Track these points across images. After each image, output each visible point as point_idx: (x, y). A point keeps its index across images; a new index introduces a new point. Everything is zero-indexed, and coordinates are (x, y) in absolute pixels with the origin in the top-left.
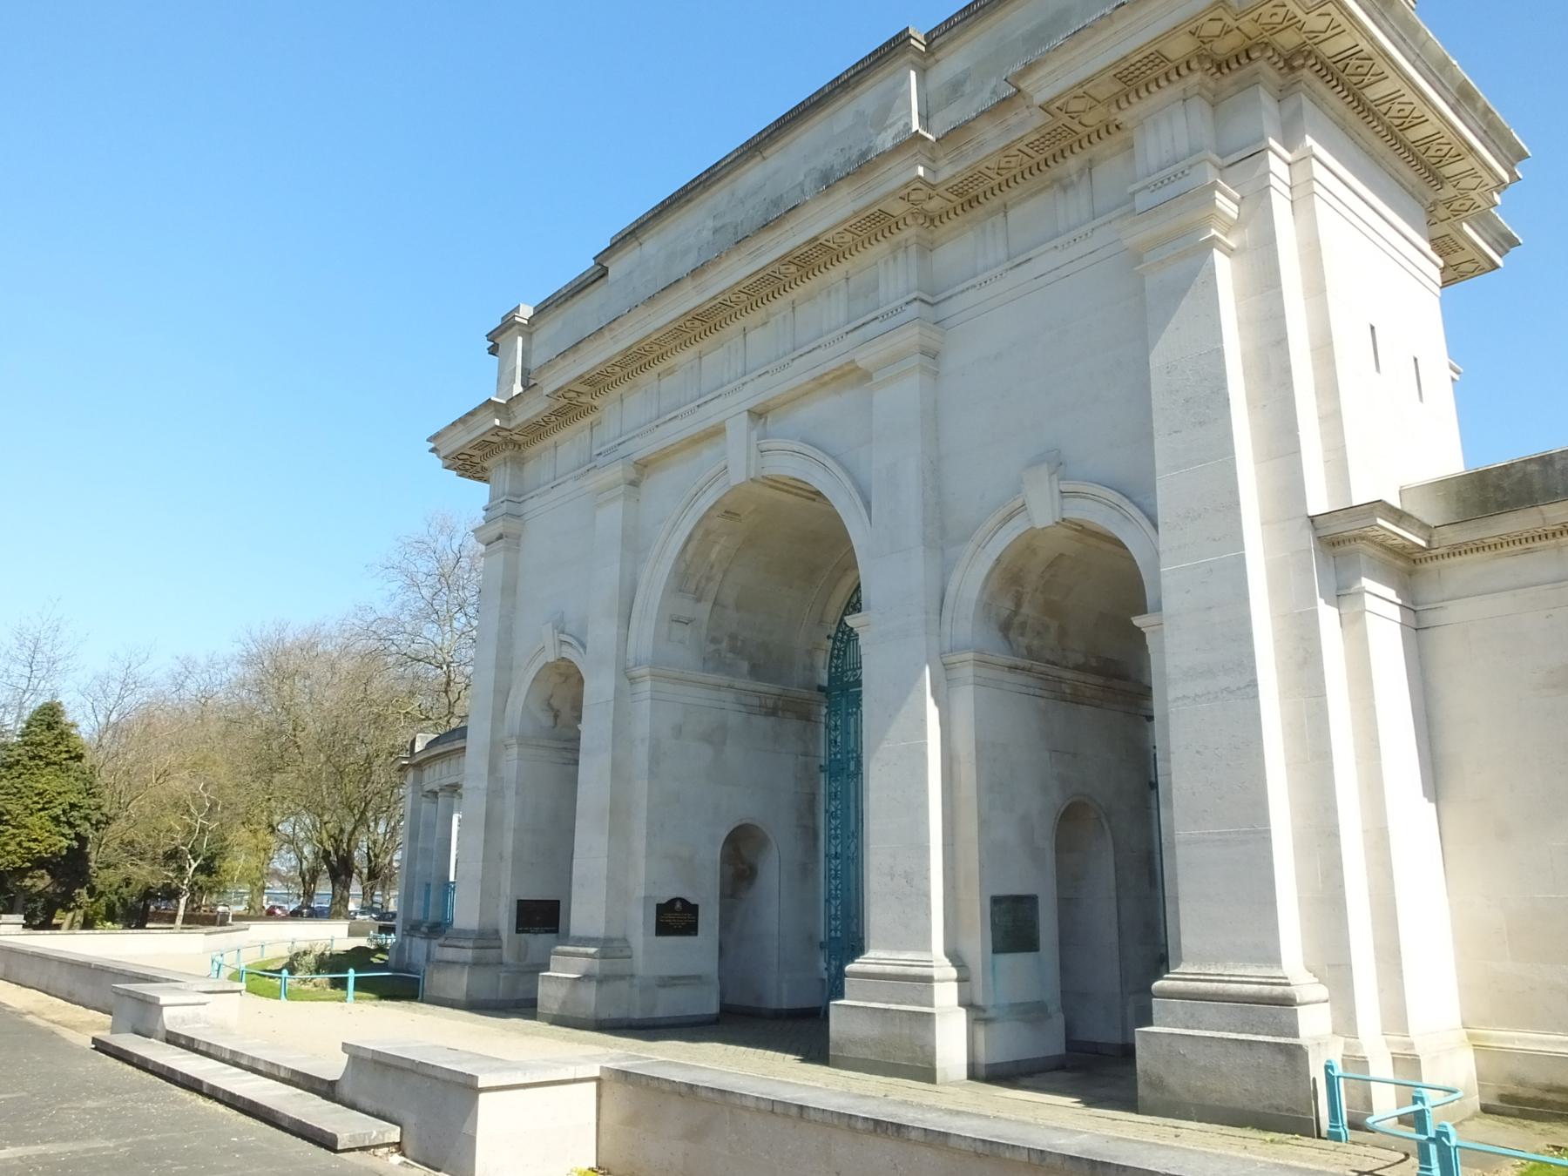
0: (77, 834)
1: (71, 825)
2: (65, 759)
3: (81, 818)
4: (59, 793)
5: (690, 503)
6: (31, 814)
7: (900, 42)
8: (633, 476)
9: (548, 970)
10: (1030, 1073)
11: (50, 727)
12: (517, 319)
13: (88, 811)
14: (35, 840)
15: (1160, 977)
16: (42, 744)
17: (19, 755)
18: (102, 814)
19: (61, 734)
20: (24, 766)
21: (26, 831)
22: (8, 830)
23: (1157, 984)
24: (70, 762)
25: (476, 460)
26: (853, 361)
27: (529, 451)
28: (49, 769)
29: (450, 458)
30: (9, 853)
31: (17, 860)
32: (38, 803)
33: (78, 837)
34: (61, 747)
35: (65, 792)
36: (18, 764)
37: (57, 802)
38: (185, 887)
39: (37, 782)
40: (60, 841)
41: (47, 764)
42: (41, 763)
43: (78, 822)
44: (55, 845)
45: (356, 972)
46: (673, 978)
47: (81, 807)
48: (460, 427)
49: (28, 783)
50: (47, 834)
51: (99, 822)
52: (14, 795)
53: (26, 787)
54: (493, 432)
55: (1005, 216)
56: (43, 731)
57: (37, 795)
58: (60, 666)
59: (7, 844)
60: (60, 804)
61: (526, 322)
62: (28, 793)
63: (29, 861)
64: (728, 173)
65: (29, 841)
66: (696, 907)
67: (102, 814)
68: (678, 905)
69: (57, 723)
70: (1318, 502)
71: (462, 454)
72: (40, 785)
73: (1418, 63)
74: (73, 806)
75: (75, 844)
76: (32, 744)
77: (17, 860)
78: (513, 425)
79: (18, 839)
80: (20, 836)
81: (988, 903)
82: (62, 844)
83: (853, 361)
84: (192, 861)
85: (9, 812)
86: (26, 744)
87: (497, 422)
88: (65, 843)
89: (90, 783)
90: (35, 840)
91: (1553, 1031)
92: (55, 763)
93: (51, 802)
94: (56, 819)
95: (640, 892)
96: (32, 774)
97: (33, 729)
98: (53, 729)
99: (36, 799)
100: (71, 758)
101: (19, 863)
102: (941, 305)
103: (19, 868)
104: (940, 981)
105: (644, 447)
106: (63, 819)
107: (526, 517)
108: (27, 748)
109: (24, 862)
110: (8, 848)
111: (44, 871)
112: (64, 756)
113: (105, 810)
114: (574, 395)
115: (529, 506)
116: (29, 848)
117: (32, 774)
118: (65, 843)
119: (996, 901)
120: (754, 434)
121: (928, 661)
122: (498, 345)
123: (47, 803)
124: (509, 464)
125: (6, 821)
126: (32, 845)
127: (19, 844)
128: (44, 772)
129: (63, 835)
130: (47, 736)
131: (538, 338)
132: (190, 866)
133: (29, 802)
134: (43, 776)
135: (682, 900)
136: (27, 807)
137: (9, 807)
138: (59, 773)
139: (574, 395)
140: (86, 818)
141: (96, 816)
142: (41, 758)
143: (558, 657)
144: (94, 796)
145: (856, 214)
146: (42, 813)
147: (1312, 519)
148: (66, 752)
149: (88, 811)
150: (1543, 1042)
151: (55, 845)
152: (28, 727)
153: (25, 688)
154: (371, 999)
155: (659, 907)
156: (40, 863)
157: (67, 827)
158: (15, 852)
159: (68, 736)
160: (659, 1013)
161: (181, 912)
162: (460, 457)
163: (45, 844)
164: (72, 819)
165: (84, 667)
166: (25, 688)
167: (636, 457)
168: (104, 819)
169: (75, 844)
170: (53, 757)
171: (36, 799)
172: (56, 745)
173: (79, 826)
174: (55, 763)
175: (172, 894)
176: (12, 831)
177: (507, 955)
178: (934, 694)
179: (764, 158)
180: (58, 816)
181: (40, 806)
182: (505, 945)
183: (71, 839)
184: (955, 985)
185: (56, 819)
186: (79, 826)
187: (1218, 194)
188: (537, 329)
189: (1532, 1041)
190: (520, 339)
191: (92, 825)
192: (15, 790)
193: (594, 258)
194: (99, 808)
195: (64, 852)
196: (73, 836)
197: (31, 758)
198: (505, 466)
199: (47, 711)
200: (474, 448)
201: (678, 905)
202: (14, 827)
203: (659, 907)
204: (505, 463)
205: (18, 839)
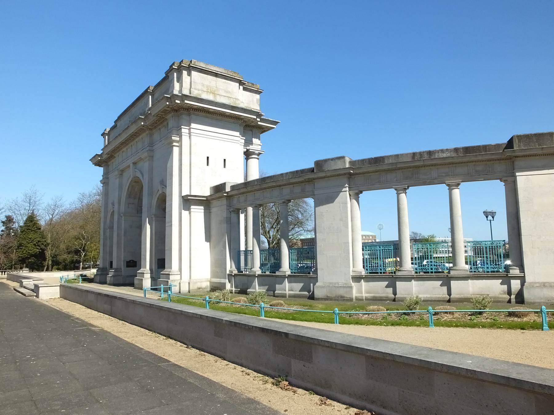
0: (41, 248)
1: (39, 246)
2: (36, 229)
3: (41, 244)
4: (35, 238)
5: (128, 181)
6: (29, 244)
7: (146, 92)
8: (120, 173)
9: (137, 277)
10: (130, 285)
11: (31, 221)
12: (148, 91)
13: (43, 242)
14: (30, 250)
15: (162, 272)
16: (29, 226)
17: (24, 229)
18: (46, 243)
19: (35, 223)
20: (26, 232)
21: (27, 248)
22: (23, 248)
23: (138, 272)
24: (37, 230)
25: (164, 116)
26: (141, 158)
27: (109, 163)
28: (32, 232)
29: (155, 116)
30: (24, 253)
31: (26, 255)
32: (30, 241)
33: (41, 249)
34: (35, 227)
35: (36, 238)
36: (24, 231)
37: (35, 240)
38: (81, 260)
39: (29, 236)
40: (36, 250)
41: (32, 231)
42: (30, 231)
43: (41, 245)
44: (35, 251)
45: (163, 286)
46: (130, 276)
47: (41, 241)
48: (94, 159)
49: (27, 236)
50: (33, 248)
51: (46, 245)
52: (24, 239)
53: (27, 237)
54: (167, 107)
55: (160, 131)
56: (30, 223)
57: (29, 239)
58: (37, 203)
59: (23, 251)
60: (36, 241)
61: (151, 91)
62: (27, 239)
63: (29, 255)
64: (129, 110)
65: (29, 250)
66: (136, 262)
67: (46, 243)
68: (132, 261)
69: (33, 220)
70: (184, 194)
71: (159, 114)
72: (30, 236)
73: (217, 106)
74: (39, 241)
75: (41, 251)
76: (27, 226)
77: (26, 255)
78: (103, 159)
79: (26, 250)
80: (26, 249)
81: (157, 260)
82: (37, 251)
83: (141, 158)
84: (83, 253)
85: (23, 243)
86: (26, 226)
87: (99, 158)
88: (38, 250)
89: (43, 235)
90: (30, 250)
91: (218, 278)
92: (33, 231)
93: (33, 240)
94: (35, 245)
95: (123, 259)
96: (28, 234)
97: (27, 222)
98: (32, 222)
99: (29, 240)
100: (38, 229)
101: (27, 256)
102: (154, 147)
103: (27, 257)
104: (171, 275)
105: (121, 167)
106: (37, 244)
107: (154, 151)
108: (26, 227)
109: (28, 256)
110: (24, 252)
111: (33, 258)
112: (36, 229)
113: (47, 242)
114: (160, 115)
115: (154, 147)
116: (29, 252)
117: (28, 234)
118: (38, 250)
119: (158, 260)
120: (134, 168)
121: (148, 217)
122: (169, 76)
123: (32, 241)
124: (173, 117)
125: (23, 246)
126: (29, 251)
127: (26, 251)
128: (31, 233)
129: (37, 249)
130: (31, 224)
131: (111, 136)
132: (82, 254)
133: (28, 241)
134: (31, 234)
135: (133, 260)
136: (27, 242)
137: (23, 242)
138: (35, 233)
139: (160, 115)
140: (42, 244)
141: (45, 243)
142: (30, 230)
143: (162, 192)
144: (44, 238)
145: (137, 129)
146: (31, 243)
147: (183, 197)
148: (36, 228)
149: (43, 242)
150: (217, 280)
151: (35, 251)
152: (26, 222)
153: (28, 209)
154: (86, 283)
155: (127, 262)
156: (32, 256)
157: (38, 247)
158: (25, 253)
159: (36, 224)
160: (127, 282)
161: (81, 267)
162: (159, 115)
163: (33, 251)
164: (39, 245)
165: (44, 203)
166: (28, 209)
167: (120, 169)
168: (47, 244)
169: (41, 251)
170: (33, 229)
171: (29, 240)
172: (33, 226)
173: (41, 246)
174: (33, 231)
175: (79, 262)
176: (24, 248)
177: (123, 273)
178: (149, 223)
179: (135, 107)
180: (35, 244)
181: (30, 242)
182: (123, 271)
183: (40, 250)
184: (150, 274)
185: (35, 245)
186: (41, 246)
187: (173, 137)
188: (155, 93)
189: (218, 280)
190: (150, 97)
191: (44, 246)
192: (24, 238)
193: (165, 73)
194: (45, 241)
195: (38, 253)
196: (40, 249)
197: (27, 230)
198: (172, 118)
199: (30, 217)
200: (162, 112)
201: (132, 261)
202: (25, 247)
203: (127, 262)
204: (172, 117)
205: (26, 250)
